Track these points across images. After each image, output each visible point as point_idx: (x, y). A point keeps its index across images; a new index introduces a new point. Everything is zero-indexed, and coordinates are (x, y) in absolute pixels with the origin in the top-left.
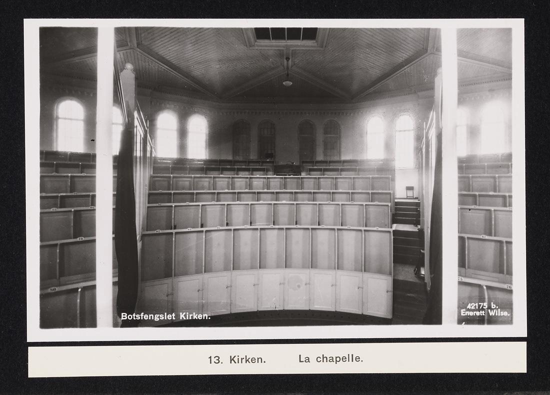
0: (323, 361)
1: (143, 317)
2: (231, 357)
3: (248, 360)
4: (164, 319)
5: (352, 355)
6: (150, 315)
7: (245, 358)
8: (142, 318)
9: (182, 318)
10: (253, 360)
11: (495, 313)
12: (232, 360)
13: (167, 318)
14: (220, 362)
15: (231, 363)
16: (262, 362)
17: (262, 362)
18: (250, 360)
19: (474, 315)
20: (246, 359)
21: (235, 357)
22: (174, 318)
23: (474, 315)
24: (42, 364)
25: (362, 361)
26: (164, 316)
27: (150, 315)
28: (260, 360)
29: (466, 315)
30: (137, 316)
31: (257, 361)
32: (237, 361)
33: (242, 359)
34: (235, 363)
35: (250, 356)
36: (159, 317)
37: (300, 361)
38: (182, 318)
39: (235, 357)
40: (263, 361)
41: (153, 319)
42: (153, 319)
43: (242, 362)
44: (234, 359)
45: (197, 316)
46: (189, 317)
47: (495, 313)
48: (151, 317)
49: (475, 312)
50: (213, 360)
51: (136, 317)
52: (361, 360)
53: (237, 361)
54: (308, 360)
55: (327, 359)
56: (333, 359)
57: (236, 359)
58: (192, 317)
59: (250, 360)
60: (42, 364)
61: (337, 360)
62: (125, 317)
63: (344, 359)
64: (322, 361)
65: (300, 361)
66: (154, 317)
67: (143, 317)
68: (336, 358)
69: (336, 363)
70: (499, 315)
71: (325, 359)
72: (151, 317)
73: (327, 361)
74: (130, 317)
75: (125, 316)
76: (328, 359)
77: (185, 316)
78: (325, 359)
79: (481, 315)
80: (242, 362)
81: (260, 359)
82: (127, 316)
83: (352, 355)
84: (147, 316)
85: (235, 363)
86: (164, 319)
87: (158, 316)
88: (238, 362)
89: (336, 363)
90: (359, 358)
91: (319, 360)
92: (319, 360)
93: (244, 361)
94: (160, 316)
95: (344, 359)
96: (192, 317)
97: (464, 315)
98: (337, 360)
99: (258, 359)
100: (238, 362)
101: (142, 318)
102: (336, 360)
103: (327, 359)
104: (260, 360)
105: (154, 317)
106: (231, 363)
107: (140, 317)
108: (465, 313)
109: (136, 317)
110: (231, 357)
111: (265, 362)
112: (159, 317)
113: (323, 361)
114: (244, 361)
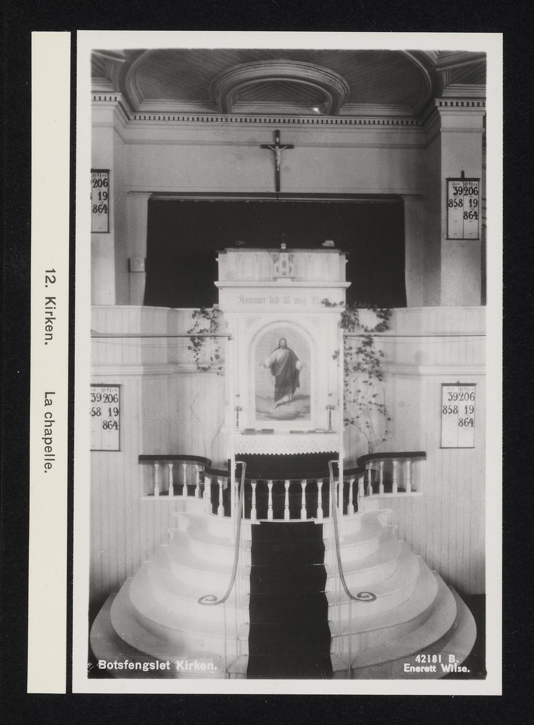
0: (46, 421)
1: (128, 665)
2: (55, 298)
3: (49, 321)
4: (129, 662)
5: (54, 460)
6: (137, 664)
7: (52, 317)
8: (126, 668)
9: (180, 668)
10: (49, 328)
11: (450, 669)
12: (50, 299)
13: (159, 668)
14: (46, 470)
15: (46, 298)
16: (46, 339)
17: (46, 339)
18: (49, 324)
19: (422, 671)
20: (51, 318)
21: (54, 303)
22: (435, 671)
23: (422, 671)
24: (48, 49)
25: (46, 472)
26: (155, 665)
27: (137, 664)
28: (49, 337)
29: (411, 671)
30: (119, 665)
31: (48, 332)
32: (48, 306)
33: (51, 313)
34: (46, 304)
35: (55, 324)
36: (149, 666)
37: (46, 393)
38: (180, 668)
39: (54, 303)
40: (47, 341)
41: (140, 668)
42: (140, 668)
43: (46, 313)
44: (49, 322)
45: (200, 666)
46: (188, 667)
47: (450, 669)
48: (138, 665)
49: (422, 668)
50: (50, 275)
51: (117, 666)
52: (47, 470)
53: (48, 306)
54: (48, 403)
55: (49, 426)
56: (48, 434)
57: (51, 305)
58: (193, 667)
59: (49, 324)
60: (48, 49)
61: (48, 439)
62: (103, 666)
63: (48, 448)
64: (47, 420)
65: (46, 393)
66: (142, 666)
67: (128, 665)
68: (50, 439)
69: (43, 438)
70: (456, 671)
71: (49, 424)
72: (138, 665)
73: (45, 426)
74: (110, 666)
75: (104, 665)
76: (49, 428)
77: (184, 665)
78: (49, 424)
79: (432, 671)
80: (46, 313)
81: (48, 466)
82: (106, 665)
83: (54, 460)
84: (133, 665)
85: (46, 304)
86: (129, 662)
87: (147, 664)
88: (46, 308)
89: (43, 438)
90: (49, 468)
91: (48, 416)
92: (48, 416)
93: (49, 316)
94: (151, 665)
95: (48, 448)
96: (193, 667)
97: (408, 671)
98: (48, 439)
99: (51, 335)
100: (46, 308)
101: (126, 668)
102: (46, 439)
103: (49, 426)
104: (49, 337)
105: (142, 666)
106: (46, 298)
107: (124, 665)
108: (409, 669)
109: (117, 666)
110: (55, 298)
111: (46, 343)
112: (149, 666)
113: (46, 421)
114: (49, 316)
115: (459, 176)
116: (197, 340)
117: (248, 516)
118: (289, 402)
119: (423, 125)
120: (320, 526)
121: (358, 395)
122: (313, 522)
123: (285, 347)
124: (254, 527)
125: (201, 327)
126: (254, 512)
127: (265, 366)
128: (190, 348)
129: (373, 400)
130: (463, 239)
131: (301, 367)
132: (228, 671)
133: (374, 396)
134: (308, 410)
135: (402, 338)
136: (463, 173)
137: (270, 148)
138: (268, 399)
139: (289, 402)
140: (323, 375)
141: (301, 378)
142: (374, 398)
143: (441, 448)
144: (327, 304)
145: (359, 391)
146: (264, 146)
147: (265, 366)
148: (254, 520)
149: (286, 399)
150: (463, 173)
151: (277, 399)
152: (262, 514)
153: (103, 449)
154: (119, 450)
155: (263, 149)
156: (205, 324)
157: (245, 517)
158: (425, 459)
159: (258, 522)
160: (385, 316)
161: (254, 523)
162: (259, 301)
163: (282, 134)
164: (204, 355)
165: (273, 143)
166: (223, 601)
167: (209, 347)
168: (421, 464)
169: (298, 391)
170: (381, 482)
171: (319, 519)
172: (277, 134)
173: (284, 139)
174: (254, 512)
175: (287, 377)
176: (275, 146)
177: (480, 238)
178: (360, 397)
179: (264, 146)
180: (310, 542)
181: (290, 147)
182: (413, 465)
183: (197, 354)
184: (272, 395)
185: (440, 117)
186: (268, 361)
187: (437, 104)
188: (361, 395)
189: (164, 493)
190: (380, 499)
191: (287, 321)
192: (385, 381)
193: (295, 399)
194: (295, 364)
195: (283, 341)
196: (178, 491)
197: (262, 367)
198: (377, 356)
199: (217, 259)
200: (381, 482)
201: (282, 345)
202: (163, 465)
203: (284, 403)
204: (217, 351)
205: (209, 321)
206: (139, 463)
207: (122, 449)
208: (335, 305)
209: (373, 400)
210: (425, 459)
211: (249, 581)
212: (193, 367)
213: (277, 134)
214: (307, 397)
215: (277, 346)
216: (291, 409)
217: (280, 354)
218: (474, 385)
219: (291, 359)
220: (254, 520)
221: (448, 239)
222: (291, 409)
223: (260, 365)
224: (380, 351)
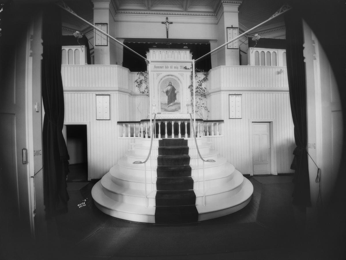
115: (231, 27)
116: (140, 84)
117: (157, 137)
118: (173, 105)
119: (216, 16)
120: (186, 141)
121: (197, 104)
122: (183, 139)
123: (171, 85)
124: (160, 141)
125: (141, 79)
126: (160, 135)
127: (164, 92)
128: (137, 86)
129: (203, 106)
130: (233, 49)
131: (177, 92)
132: (147, 197)
133: (203, 104)
134: (180, 108)
135: (199, 150)
136: (232, 26)
137: (164, 23)
138: (165, 104)
139: (173, 105)
140: (184, 96)
141: (177, 96)
142: (203, 105)
143: (230, 119)
144: (186, 68)
145: (198, 102)
146: (163, 23)
147: (164, 92)
148: (160, 138)
149: (172, 104)
150: (232, 26)
151: (168, 105)
152: (163, 134)
153: (104, 119)
154: (110, 120)
155: (162, 24)
156: (142, 78)
157: (156, 138)
158: (224, 123)
159: (161, 139)
160: (206, 75)
161: (160, 139)
162: (161, 67)
163: (168, 19)
164: (142, 89)
165: (165, 21)
166: (145, 162)
167: (144, 86)
168: (222, 125)
169: (176, 101)
170: (208, 131)
171: (186, 138)
172: (167, 18)
173: (170, 20)
174: (160, 135)
175: (172, 95)
176: (167, 22)
177: (239, 48)
178: (198, 104)
179: (163, 23)
180: (182, 149)
181: (171, 23)
182: (219, 125)
183: (140, 88)
184: (167, 102)
185: (223, 7)
186: (165, 91)
187: (222, 2)
188: (198, 103)
189: (127, 136)
190: (207, 138)
191: (172, 75)
192: (207, 99)
193: (175, 104)
194: (175, 91)
195: (170, 83)
196: (132, 136)
197: (163, 92)
198: (204, 89)
199: (146, 55)
200: (208, 131)
201: (170, 84)
202: (127, 126)
203: (171, 106)
204: (146, 86)
205: (144, 77)
206: (99, 63)
207: (111, 119)
208: (189, 69)
209: (203, 106)
210: (224, 123)
211: (158, 150)
212: (138, 93)
213: (167, 18)
214: (179, 104)
215: (168, 85)
216: (173, 108)
217: (169, 88)
218: (241, 95)
219: (173, 89)
220: (160, 138)
221: (228, 49)
222: (173, 108)
223: (162, 92)
224: (205, 88)
